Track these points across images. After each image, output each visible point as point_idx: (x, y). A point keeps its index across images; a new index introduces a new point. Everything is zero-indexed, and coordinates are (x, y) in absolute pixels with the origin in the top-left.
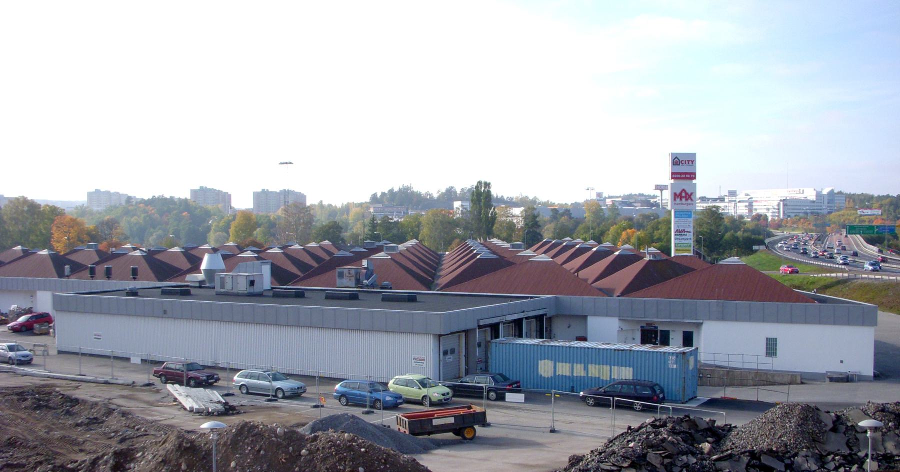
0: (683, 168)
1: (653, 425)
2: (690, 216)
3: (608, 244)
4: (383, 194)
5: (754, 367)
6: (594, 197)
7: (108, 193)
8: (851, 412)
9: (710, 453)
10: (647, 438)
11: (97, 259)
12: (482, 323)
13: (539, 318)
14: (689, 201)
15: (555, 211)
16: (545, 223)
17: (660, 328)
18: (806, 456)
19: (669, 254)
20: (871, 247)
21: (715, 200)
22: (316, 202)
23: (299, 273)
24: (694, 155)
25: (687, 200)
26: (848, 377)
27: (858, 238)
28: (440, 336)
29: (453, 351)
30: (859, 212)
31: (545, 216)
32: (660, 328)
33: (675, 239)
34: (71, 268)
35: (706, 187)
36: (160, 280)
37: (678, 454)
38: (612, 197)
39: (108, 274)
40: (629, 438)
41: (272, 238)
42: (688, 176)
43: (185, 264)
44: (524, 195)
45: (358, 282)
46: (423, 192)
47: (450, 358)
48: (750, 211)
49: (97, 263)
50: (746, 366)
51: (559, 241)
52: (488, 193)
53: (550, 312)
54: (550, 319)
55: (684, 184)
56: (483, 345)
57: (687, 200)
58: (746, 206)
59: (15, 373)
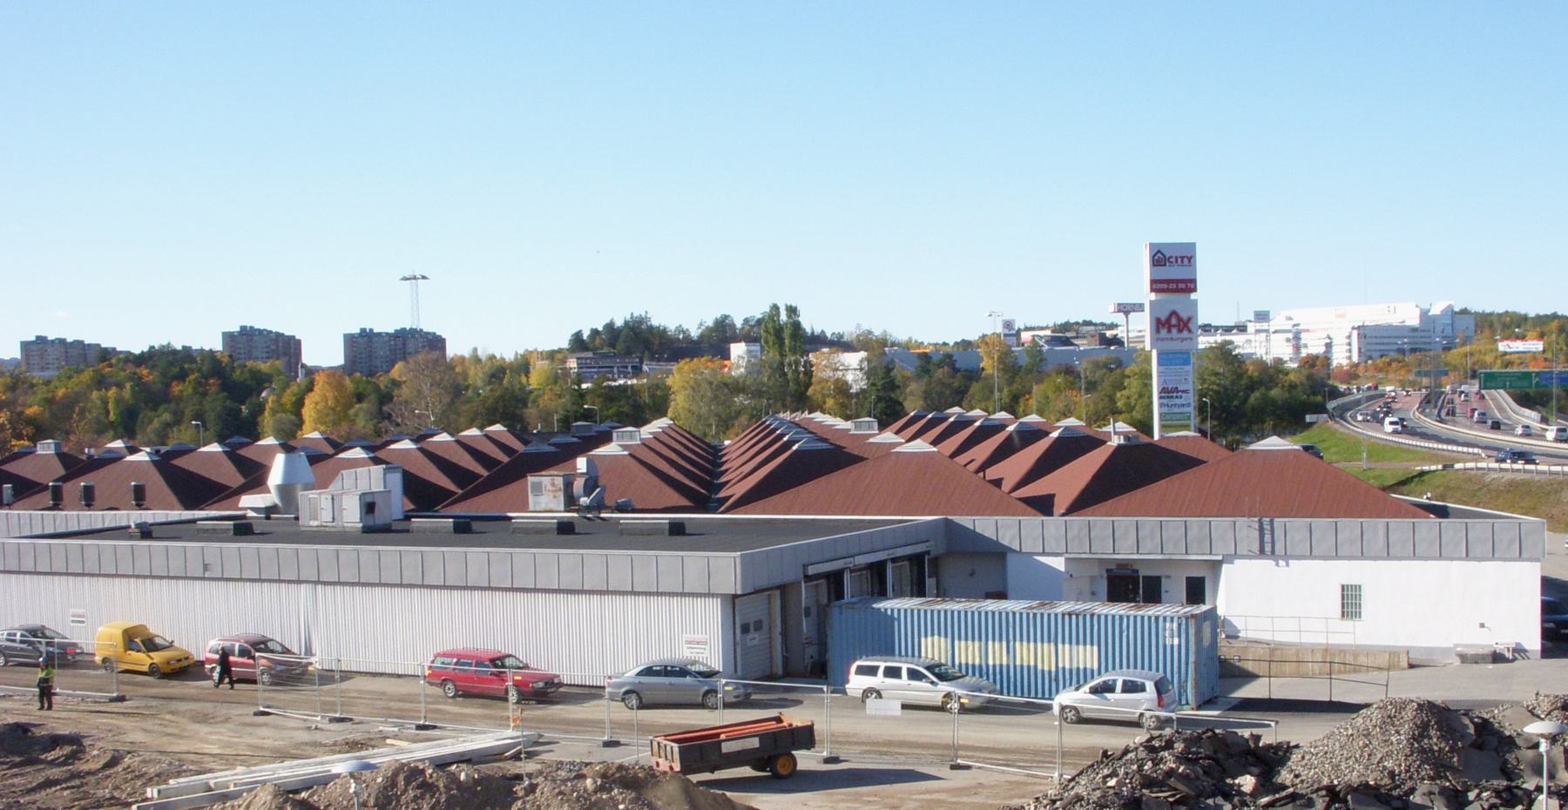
0: (1173, 272)
1: (1150, 748)
2: (1186, 362)
3: (1033, 418)
4: (595, 332)
5: (1321, 639)
6: (999, 329)
7: (62, 341)
8: (1508, 713)
9: (1255, 794)
10: (1140, 767)
11: (62, 472)
12: (811, 570)
13: (917, 560)
14: (1185, 334)
15: (925, 357)
16: (907, 379)
17: (1143, 572)
18: (1431, 793)
19: (1151, 435)
20: (1527, 412)
21: (1228, 330)
22: (466, 352)
23: (452, 487)
24: (1192, 246)
25: (1180, 331)
26: (1416, 657)
27: (1502, 397)
28: (735, 596)
29: (758, 626)
30: (1502, 346)
31: (904, 370)
32: (1143, 572)
33: (1161, 405)
34: (14, 488)
35: (1213, 304)
36: (188, 507)
37: (1198, 796)
38: (1032, 329)
39: (89, 499)
40: (1106, 772)
41: (386, 422)
42: (1182, 286)
43: (230, 475)
44: (865, 327)
45: (571, 502)
46: (671, 326)
47: (755, 638)
48: (1297, 348)
49: (64, 479)
50: (1308, 639)
51: (940, 415)
52: (797, 326)
53: (934, 547)
54: (935, 562)
55: (1174, 302)
56: (814, 611)
57: (1180, 331)
58: (1288, 340)
59: (89, 677)
